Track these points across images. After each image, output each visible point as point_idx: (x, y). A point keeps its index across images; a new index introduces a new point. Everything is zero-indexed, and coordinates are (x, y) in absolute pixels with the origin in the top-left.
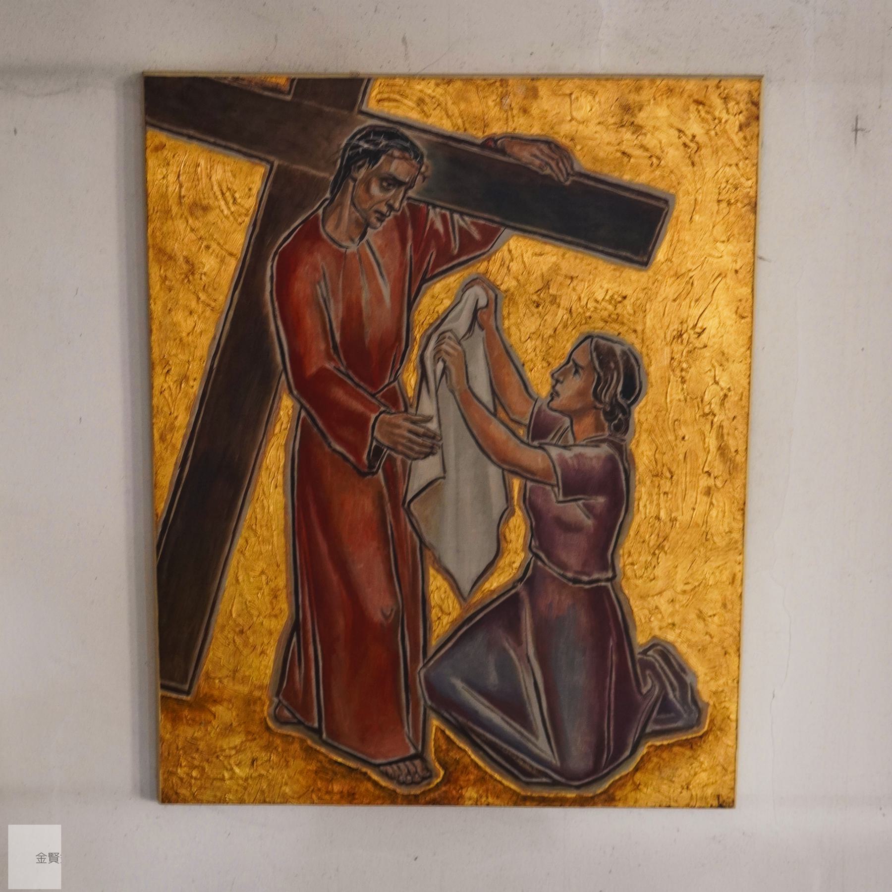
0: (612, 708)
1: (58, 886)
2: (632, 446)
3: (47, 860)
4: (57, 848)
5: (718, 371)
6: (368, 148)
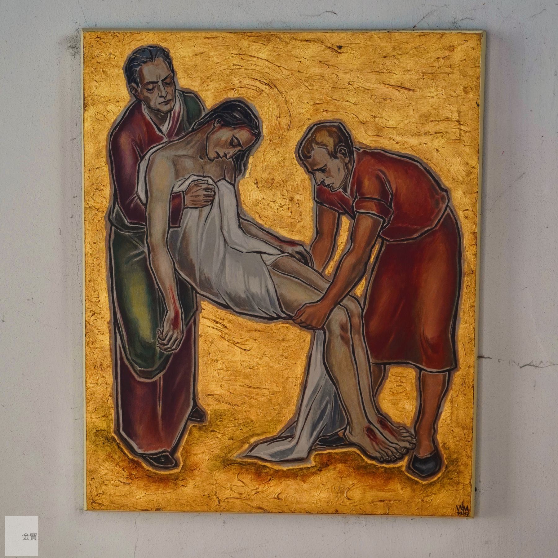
0: (161, 396)
1: (37, 554)
4: (36, 531)
5: (462, 127)
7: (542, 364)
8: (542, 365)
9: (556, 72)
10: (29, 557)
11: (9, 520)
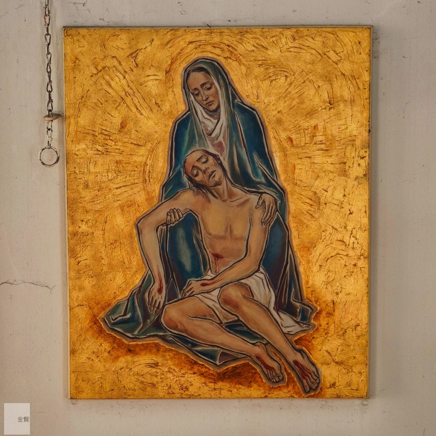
2: (214, 92)
3: (23, 420)
4: (28, 415)
6: (297, 312)
7: (16, 282)
8: (15, 283)
9: (18, 60)
10: (18, 435)
11: (7, 406)
